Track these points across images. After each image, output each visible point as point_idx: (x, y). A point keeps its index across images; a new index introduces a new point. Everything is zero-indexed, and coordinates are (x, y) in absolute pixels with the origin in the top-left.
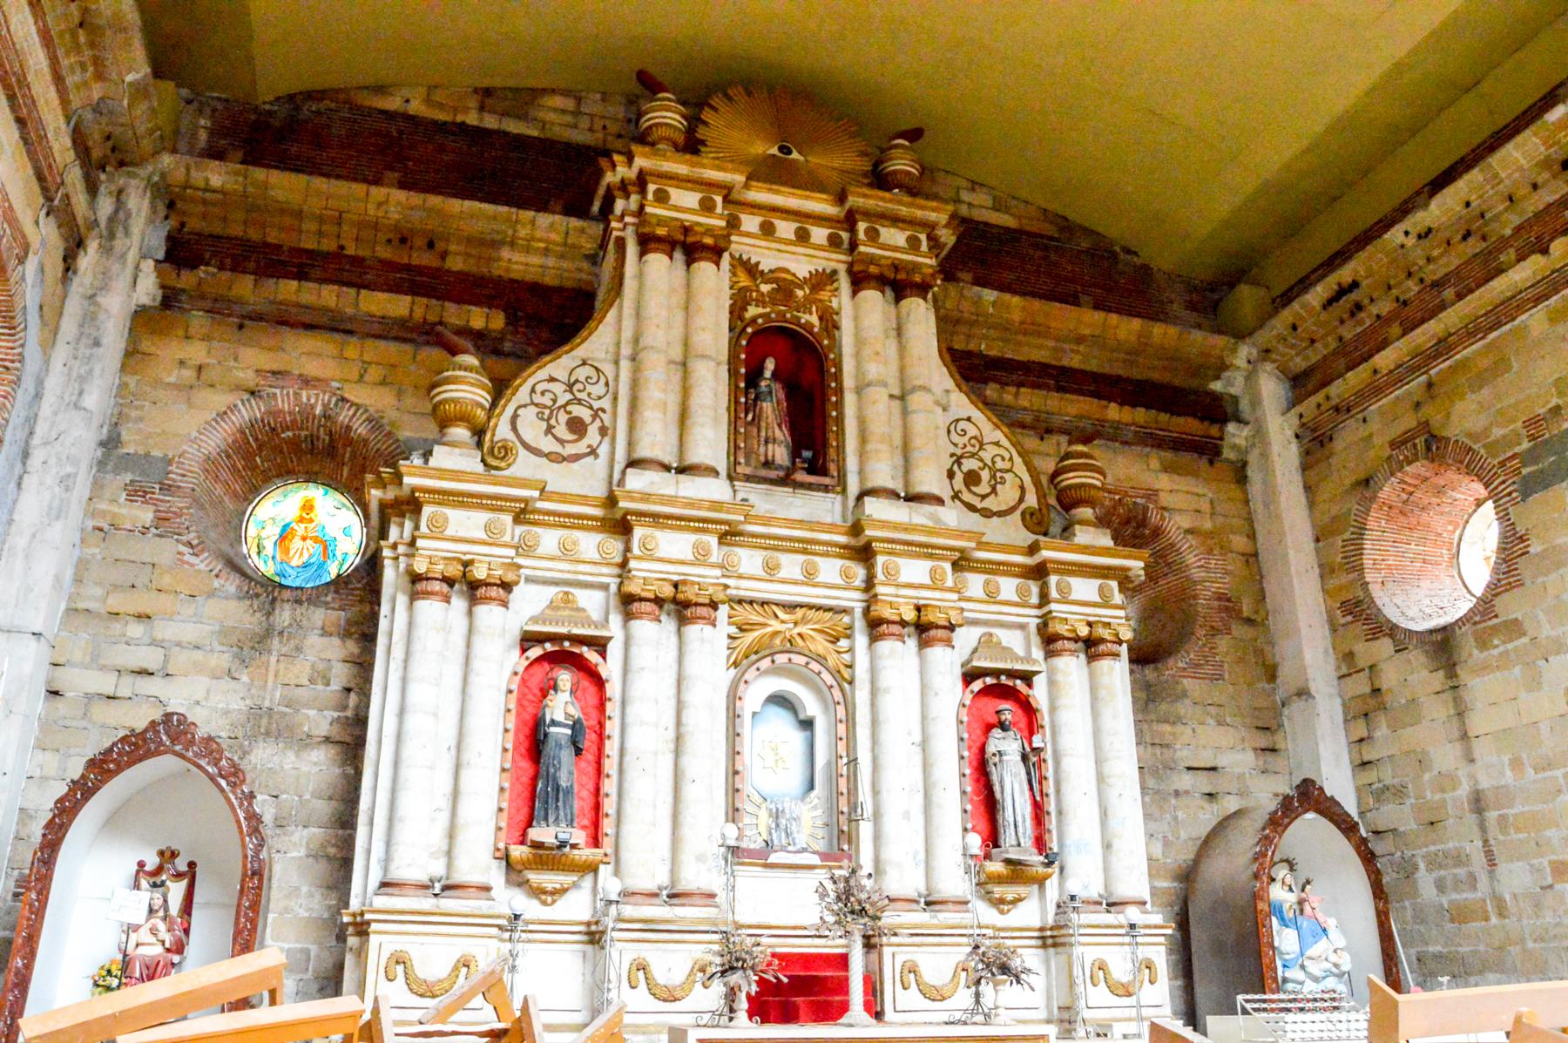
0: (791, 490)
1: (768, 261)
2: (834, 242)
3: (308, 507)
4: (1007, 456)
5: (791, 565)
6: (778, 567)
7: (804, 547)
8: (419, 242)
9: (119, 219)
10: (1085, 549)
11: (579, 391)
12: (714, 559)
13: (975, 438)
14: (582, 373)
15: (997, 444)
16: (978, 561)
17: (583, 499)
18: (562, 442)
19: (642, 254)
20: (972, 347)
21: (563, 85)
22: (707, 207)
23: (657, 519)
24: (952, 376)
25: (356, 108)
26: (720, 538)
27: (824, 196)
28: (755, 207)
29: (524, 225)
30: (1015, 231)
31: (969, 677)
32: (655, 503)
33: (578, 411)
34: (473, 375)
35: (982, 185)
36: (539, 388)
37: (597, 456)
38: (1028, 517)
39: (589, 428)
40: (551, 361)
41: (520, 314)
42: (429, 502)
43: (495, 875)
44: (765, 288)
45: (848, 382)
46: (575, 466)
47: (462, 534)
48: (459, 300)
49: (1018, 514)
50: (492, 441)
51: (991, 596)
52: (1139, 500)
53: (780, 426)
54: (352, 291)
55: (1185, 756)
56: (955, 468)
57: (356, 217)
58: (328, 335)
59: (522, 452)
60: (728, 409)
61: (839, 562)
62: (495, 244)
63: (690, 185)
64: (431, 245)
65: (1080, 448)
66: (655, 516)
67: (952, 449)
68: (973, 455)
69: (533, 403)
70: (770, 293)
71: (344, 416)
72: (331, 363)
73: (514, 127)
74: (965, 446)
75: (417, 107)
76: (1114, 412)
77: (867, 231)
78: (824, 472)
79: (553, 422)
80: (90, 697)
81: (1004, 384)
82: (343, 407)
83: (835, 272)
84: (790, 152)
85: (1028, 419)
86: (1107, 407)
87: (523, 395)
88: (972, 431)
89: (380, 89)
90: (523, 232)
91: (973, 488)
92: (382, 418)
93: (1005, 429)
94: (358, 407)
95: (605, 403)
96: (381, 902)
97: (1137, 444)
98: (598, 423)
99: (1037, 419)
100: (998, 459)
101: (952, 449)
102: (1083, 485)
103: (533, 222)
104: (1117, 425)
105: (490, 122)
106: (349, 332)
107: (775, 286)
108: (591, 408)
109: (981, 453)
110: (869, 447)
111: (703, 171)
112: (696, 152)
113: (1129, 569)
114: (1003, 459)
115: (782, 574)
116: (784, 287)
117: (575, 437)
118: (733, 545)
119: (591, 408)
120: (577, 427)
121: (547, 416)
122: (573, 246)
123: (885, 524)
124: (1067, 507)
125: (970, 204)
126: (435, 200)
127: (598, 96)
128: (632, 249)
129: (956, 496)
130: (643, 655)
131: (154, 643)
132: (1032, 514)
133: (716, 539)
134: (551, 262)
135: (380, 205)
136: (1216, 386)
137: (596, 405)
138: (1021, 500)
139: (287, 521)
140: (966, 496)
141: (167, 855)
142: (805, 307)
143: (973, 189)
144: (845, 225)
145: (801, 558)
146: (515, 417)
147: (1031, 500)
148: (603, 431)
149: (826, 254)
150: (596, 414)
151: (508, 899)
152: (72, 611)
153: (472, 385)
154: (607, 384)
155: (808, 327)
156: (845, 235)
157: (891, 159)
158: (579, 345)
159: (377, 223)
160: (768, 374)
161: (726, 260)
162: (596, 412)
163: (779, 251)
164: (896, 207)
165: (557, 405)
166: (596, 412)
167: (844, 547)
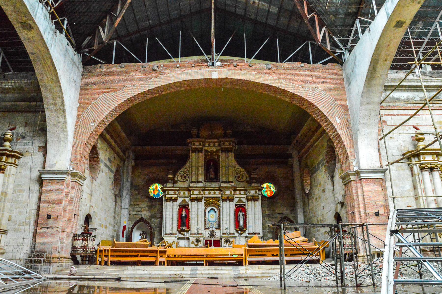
1: (209, 149)
3: (156, 187)
5: (212, 193)
6: (210, 193)
9: (129, 156)
14: (185, 170)
17: (185, 188)
18: (183, 180)
22: (200, 144)
28: (207, 142)
31: (236, 205)
43: (177, 233)
44: (209, 154)
51: (240, 194)
55: (277, 211)
59: (179, 182)
73: (177, 130)
80: (134, 215)
87: (178, 174)
88: (239, 170)
95: (188, 174)
96: (165, 236)
105: (174, 130)
115: (211, 194)
116: (212, 152)
120: (185, 177)
121: (181, 176)
123: (223, 187)
129: (236, 180)
130: (193, 206)
131: (140, 208)
136: (288, 152)
138: (246, 179)
141: (143, 232)
142: (215, 155)
147: (248, 179)
150: (187, 175)
151: (237, 235)
152: (130, 205)
155: (215, 158)
161: (203, 151)
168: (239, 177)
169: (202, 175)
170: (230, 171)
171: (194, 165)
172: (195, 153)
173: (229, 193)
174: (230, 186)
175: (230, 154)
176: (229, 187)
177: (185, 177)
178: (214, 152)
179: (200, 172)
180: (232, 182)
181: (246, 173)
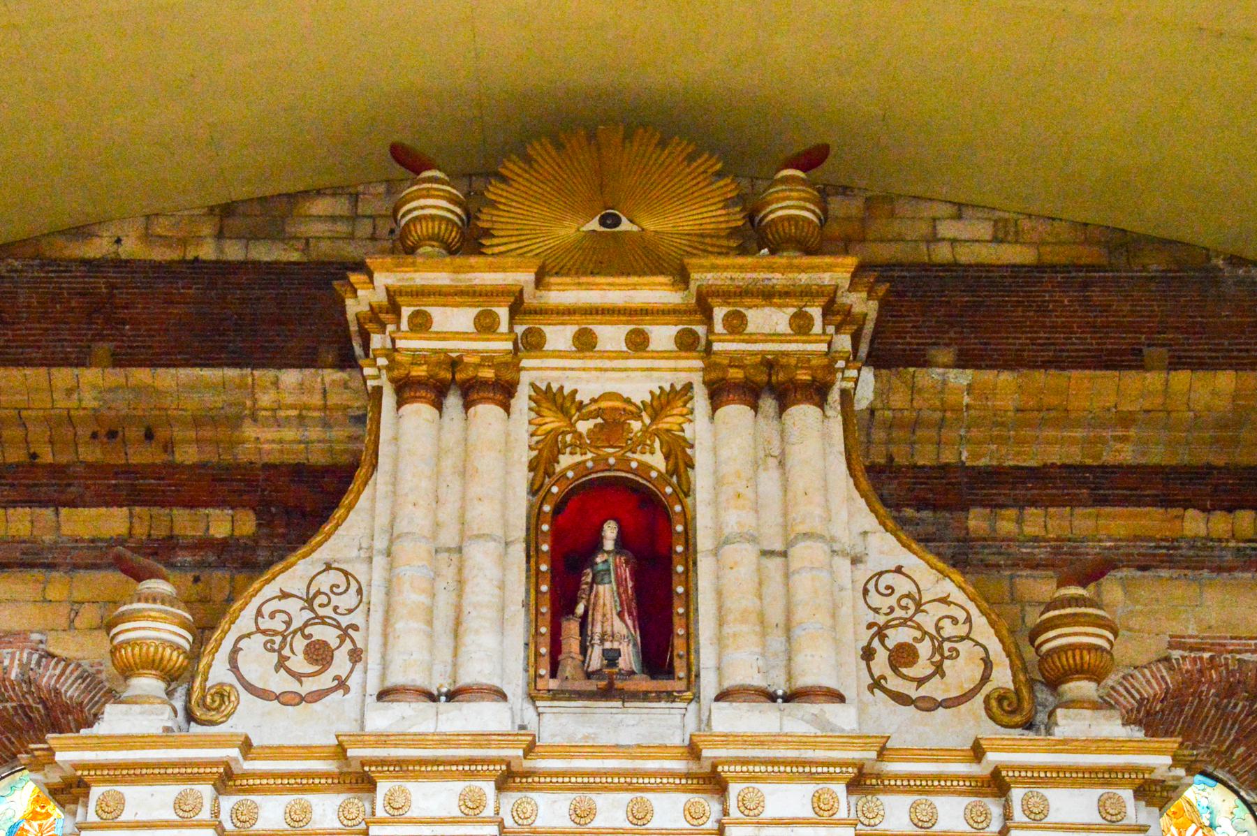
0: (619, 704)
2: (686, 343)
4: (961, 616)
7: (629, 782)
8: (135, 433)
10: (1067, 745)
11: (321, 606)
12: (842, 813)
13: (908, 596)
14: (324, 583)
15: (944, 601)
16: (896, 777)
17: (307, 752)
18: (298, 677)
19: (400, 404)
20: (948, 457)
21: (324, 180)
22: (485, 325)
23: (403, 768)
24: (873, 510)
25: (48, 263)
26: (848, 786)
27: (662, 279)
28: (568, 313)
29: (265, 389)
30: (1031, 268)
32: (396, 746)
33: (319, 632)
34: (159, 606)
35: (967, 205)
36: (266, 610)
37: (347, 690)
38: (994, 703)
39: (336, 653)
40: (282, 571)
41: (273, 509)
42: (95, 781)
44: (584, 427)
45: (704, 541)
46: (317, 706)
47: (143, 817)
48: (191, 504)
49: (979, 699)
50: (203, 689)
52: (1247, 656)
53: (620, 615)
54: (48, 513)
56: (876, 643)
57: (41, 413)
58: (17, 574)
59: (245, 696)
60: (526, 605)
61: (683, 798)
62: (235, 422)
63: (458, 299)
64: (149, 436)
65: (1074, 591)
66: (399, 762)
67: (871, 617)
68: (904, 622)
69: (259, 630)
70: (590, 432)
71: (48, 676)
72: (30, 610)
73: (264, 252)
74: (892, 610)
75: (132, 248)
76: (1194, 524)
77: (727, 318)
78: (669, 673)
79: (286, 652)
81: (995, 506)
82: (47, 666)
83: (689, 387)
84: (617, 222)
85: (1041, 553)
86: (1182, 518)
87: (245, 621)
88: (903, 586)
89: (82, 232)
90: (266, 399)
91: (904, 670)
92: (99, 672)
93: (958, 578)
94: (68, 662)
95: (357, 618)
97: (1244, 569)
98: (348, 645)
99: (1057, 550)
100: (946, 623)
101: (871, 617)
102: (1072, 647)
103: (276, 383)
104: (1208, 542)
105: (234, 252)
106: (51, 566)
107: (599, 420)
108: (338, 626)
109: (919, 618)
110: (728, 630)
111: (470, 276)
112: (478, 250)
113: (1151, 770)
114: (955, 621)
117: (317, 668)
118: (527, 789)
119: (338, 626)
120: (320, 654)
121: (278, 644)
122: (337, 407)
123: (728, 739)
124: (1053, 684)
125: (954, 241)
126: (142, 375)
127: (381, 189)
128: (388, 399)
129: (876, 684)
132: (1000, 699)
133: (492, 785)
134: (314, 433)
135: (69, 392)
137: (344, 621)
138: (985, 679)
139: (15, 820)
140: (894, 683)
143: (959, 217)
144: (698, 317)
145: (627, 797)
146: (235, 651)
147: (1003, 677)
148: (356, 655)
149: (671, 364)
150: (345, 634)
153: (155, 619)
154: (360, 591)
155: (645, 468)
156: (701, 330)
157: (769, 204)
158: (320, 544)
159: (69, 417)
160: (609, 545)
162: (345, 631)
163: (601, 370)
164: (762, 275)
165: (292, 629)
166: (345, 631)
167: (688, 776)
168: (902, 656)
169: (502, 624)
170: (804, 585)
171: (416, 519)
172: (439, 406)
173: (808, 813)
174: (810, 730)
175: (803, 414)
176: (802, 742)
177: (320, 654)
178: (638, 417)
179: (482, 590)
180: (837, 697)
181: (980, 621)
